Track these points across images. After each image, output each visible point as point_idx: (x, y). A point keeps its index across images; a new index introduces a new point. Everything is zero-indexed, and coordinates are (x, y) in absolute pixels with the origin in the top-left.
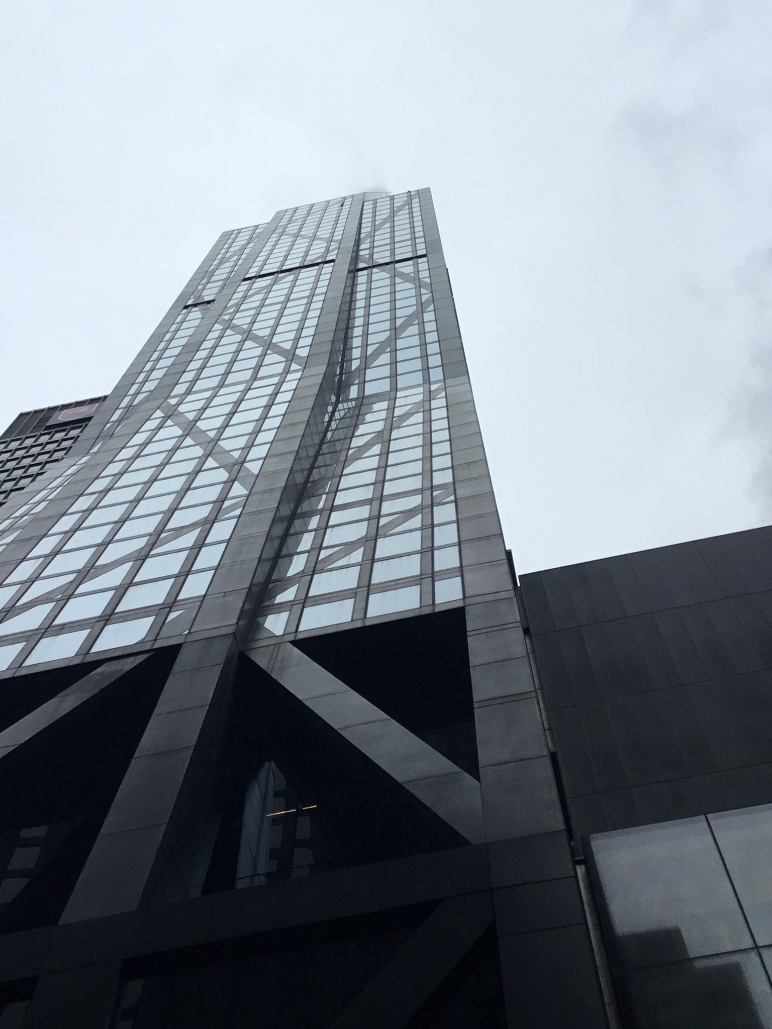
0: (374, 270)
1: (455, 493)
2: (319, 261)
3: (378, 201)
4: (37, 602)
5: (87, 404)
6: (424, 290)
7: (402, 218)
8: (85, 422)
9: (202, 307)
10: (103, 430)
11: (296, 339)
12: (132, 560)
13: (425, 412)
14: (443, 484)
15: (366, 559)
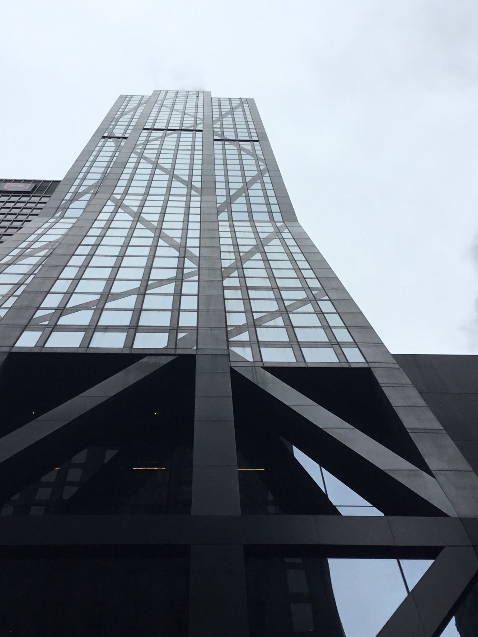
0: (225, 142)
1: (147, 284)
2: (192, 128)
3: (144, 97)
4: (81, 307)
5: (22, 183)
7: (238, 113)
8: (11, 193)
9: (114, 140)
10: (60, 204)
14: (317, 288)
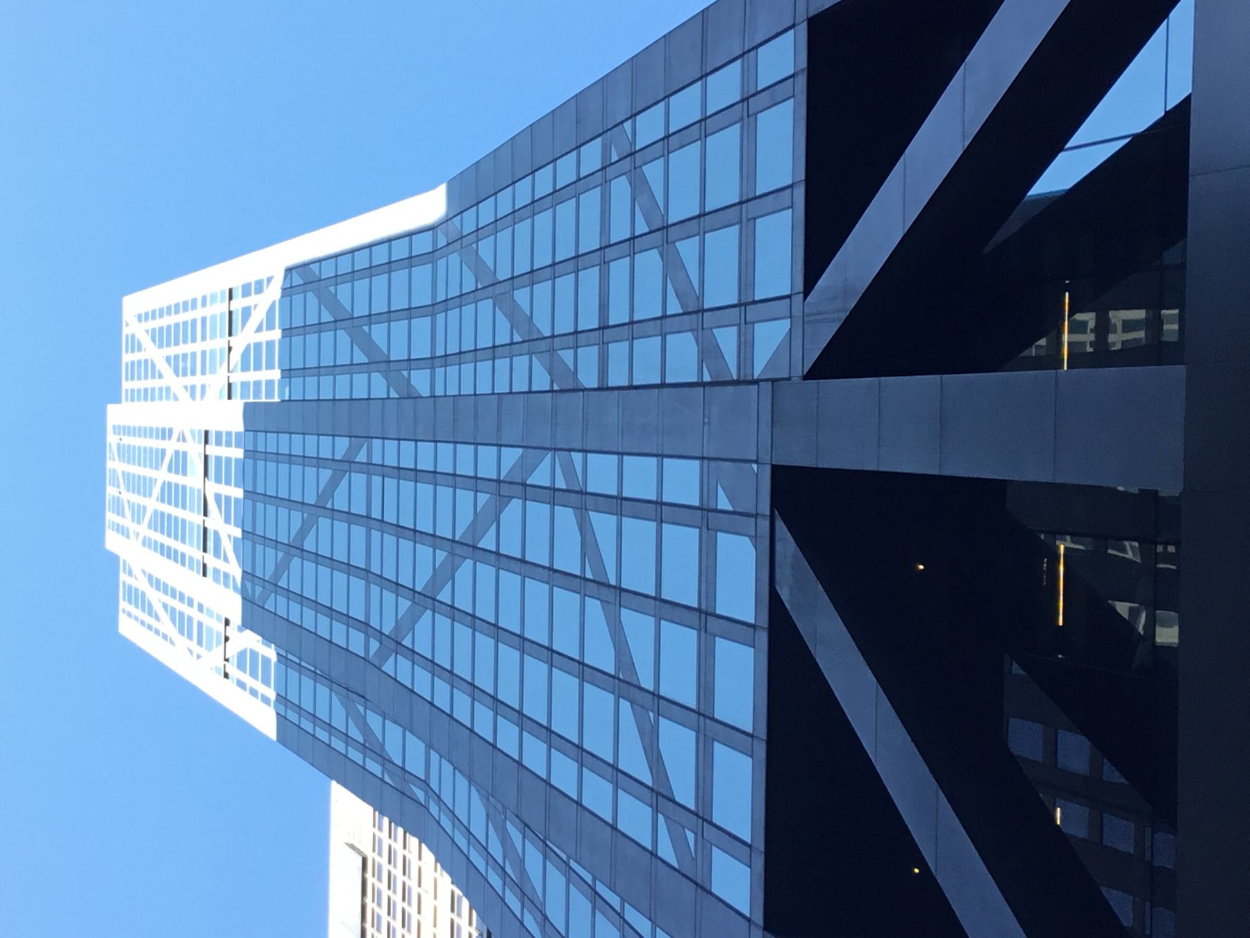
6: (281, 556)
10: (393, 787)
11: (316, 607)
12: (618, 609)
13: (478, 489)
15: (697, 622)
